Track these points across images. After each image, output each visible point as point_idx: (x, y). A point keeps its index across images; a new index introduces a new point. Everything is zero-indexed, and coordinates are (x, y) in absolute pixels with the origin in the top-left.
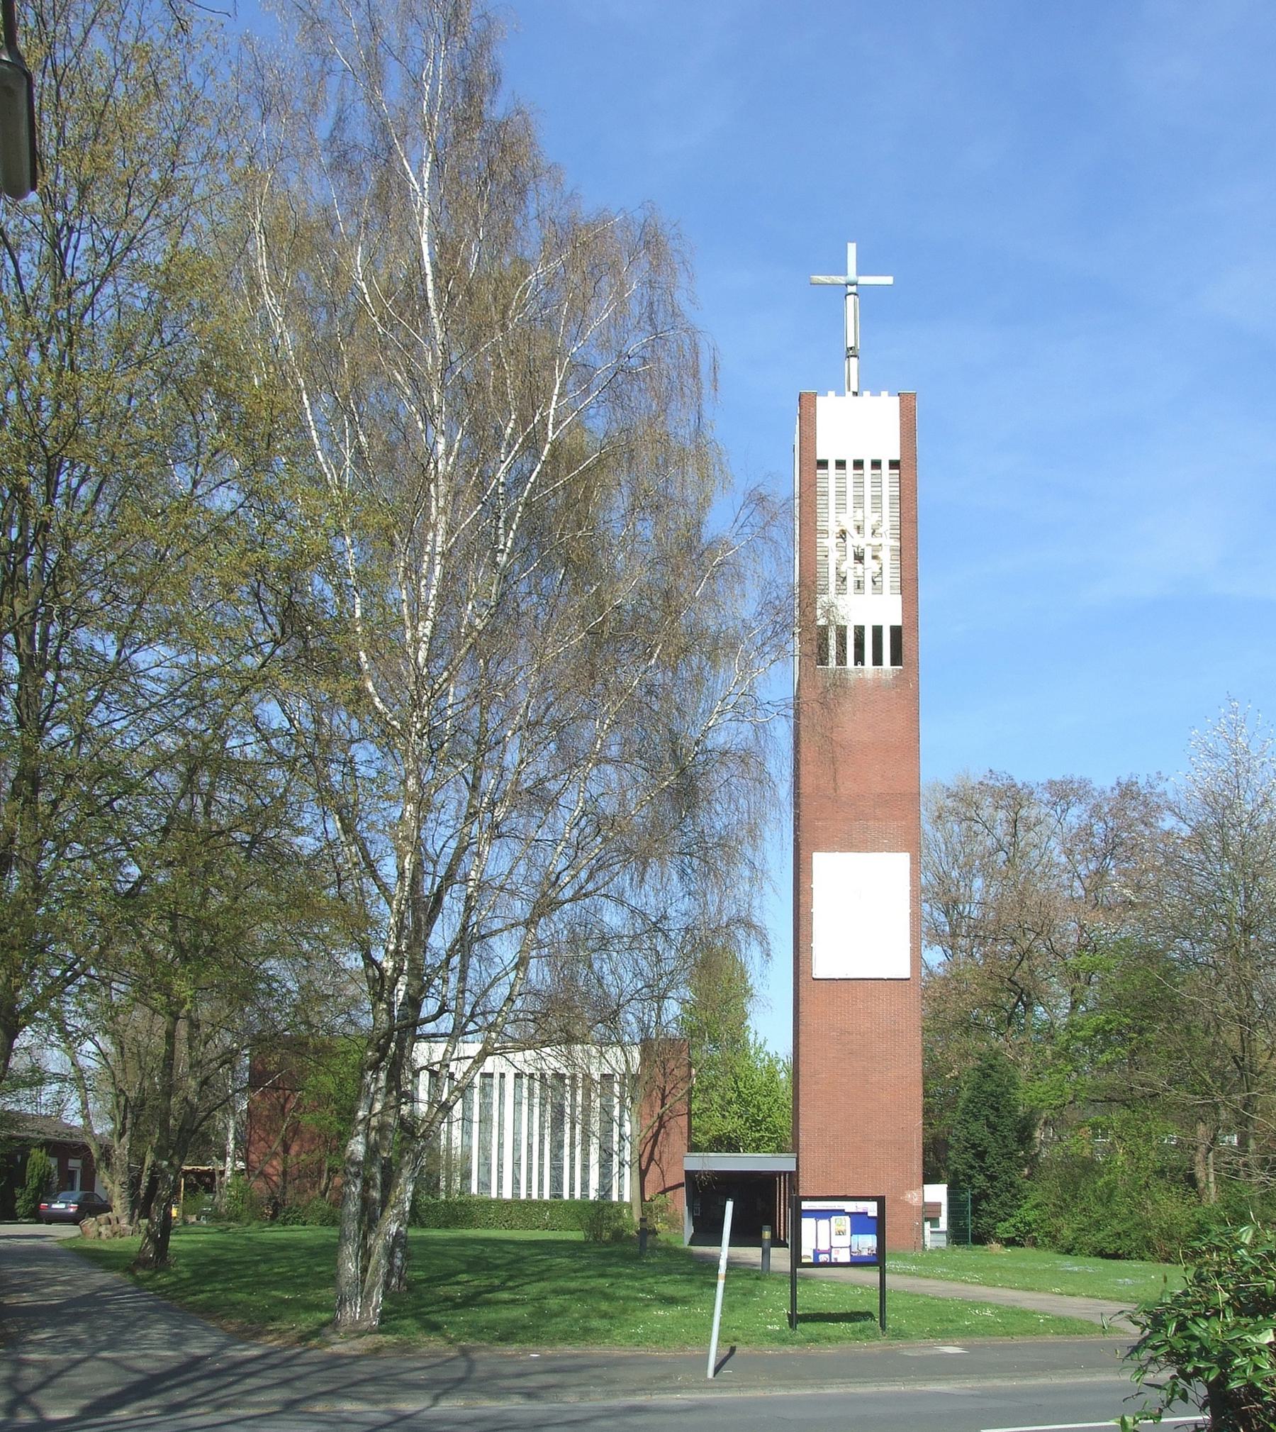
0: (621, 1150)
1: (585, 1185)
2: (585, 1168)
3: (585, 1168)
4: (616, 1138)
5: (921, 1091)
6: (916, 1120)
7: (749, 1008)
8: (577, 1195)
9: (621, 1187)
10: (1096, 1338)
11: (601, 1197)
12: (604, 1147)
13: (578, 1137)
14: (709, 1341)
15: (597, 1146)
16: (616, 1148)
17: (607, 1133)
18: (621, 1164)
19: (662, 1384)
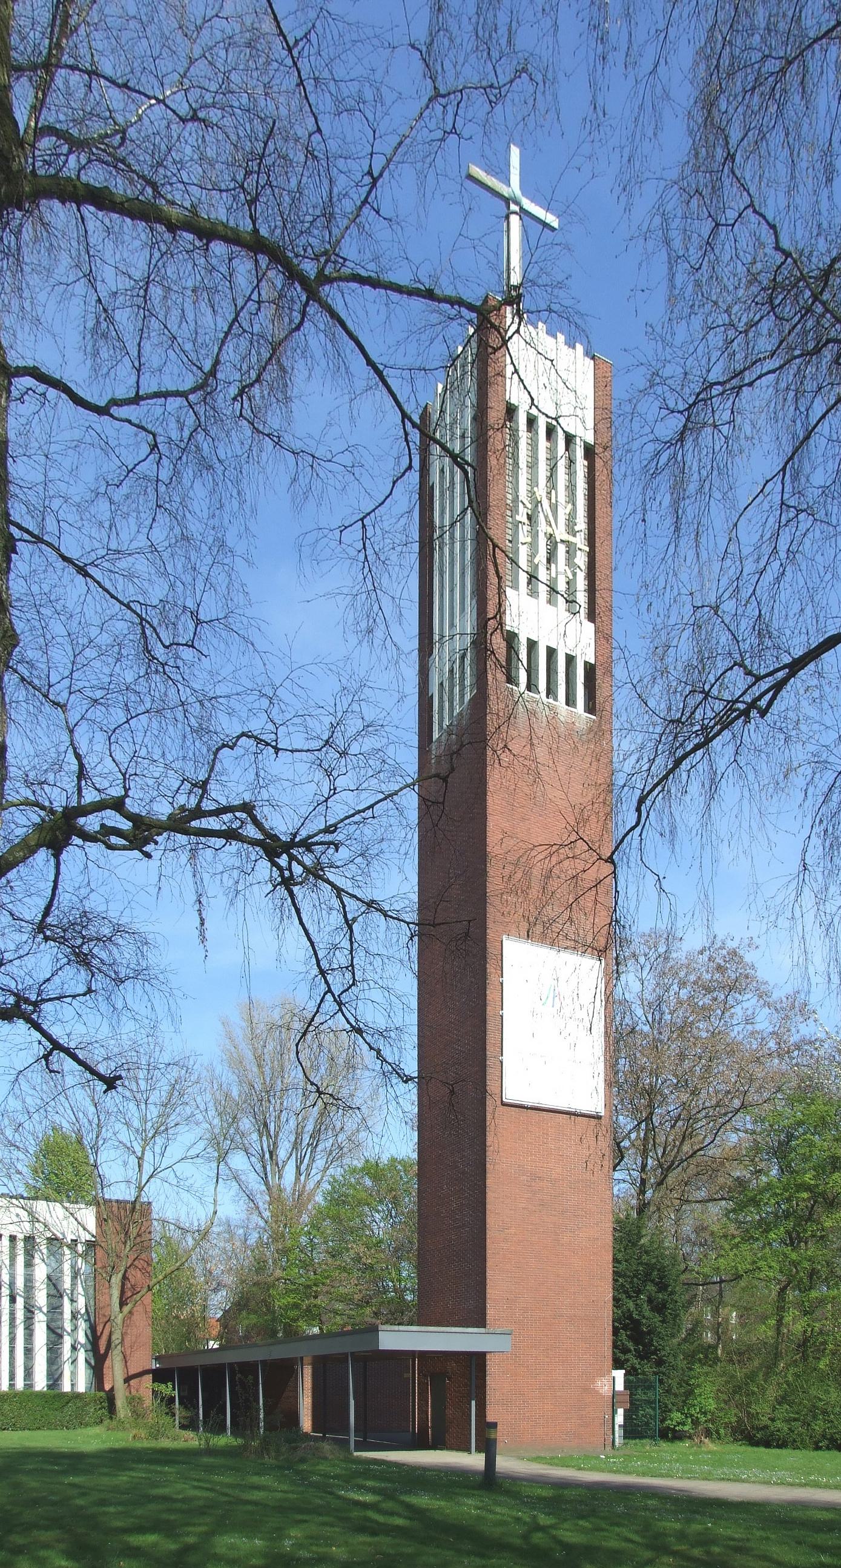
0: (75, 1328)
1: (29, 1373)
2: (29, 1352)
3: (29, 1352)
4: (67, 1315)
5: (762, 1449)
6: (605, 1292)
7: (385, 1159)
8: (20, 1384)
9: (74, 1374)
10: (5, 33)
11: (49, 1387)
12: (53, 1325)
13: (20, 1315)
14: (470, 1425)
15: (44, 1326)
16: (68, 1326)
17: (55, 1309)
18: (74, 1348)
19: (360, 1481)
